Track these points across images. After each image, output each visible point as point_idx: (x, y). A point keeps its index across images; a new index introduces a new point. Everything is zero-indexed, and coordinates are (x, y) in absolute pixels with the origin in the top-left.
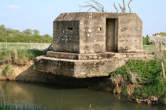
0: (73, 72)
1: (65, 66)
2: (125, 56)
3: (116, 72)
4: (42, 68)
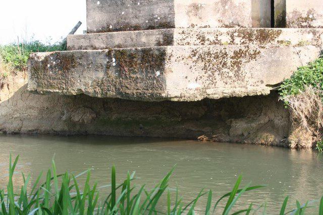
0: (161, 83)
1: (131, 64)
2: (311, 35)
3: (298, 80)
4: (55, 81)
